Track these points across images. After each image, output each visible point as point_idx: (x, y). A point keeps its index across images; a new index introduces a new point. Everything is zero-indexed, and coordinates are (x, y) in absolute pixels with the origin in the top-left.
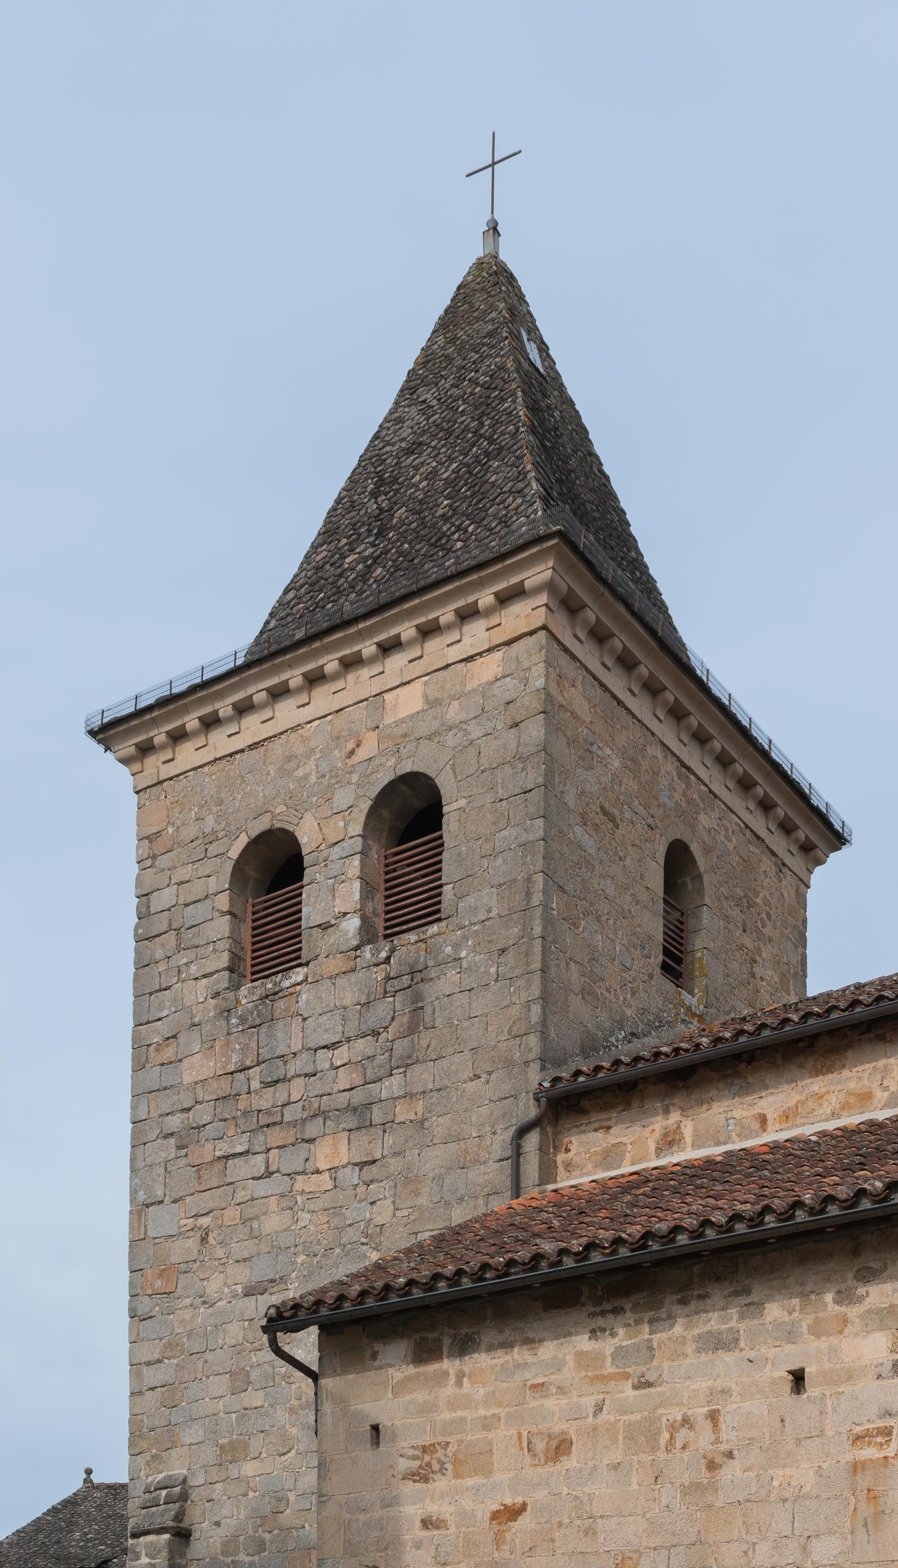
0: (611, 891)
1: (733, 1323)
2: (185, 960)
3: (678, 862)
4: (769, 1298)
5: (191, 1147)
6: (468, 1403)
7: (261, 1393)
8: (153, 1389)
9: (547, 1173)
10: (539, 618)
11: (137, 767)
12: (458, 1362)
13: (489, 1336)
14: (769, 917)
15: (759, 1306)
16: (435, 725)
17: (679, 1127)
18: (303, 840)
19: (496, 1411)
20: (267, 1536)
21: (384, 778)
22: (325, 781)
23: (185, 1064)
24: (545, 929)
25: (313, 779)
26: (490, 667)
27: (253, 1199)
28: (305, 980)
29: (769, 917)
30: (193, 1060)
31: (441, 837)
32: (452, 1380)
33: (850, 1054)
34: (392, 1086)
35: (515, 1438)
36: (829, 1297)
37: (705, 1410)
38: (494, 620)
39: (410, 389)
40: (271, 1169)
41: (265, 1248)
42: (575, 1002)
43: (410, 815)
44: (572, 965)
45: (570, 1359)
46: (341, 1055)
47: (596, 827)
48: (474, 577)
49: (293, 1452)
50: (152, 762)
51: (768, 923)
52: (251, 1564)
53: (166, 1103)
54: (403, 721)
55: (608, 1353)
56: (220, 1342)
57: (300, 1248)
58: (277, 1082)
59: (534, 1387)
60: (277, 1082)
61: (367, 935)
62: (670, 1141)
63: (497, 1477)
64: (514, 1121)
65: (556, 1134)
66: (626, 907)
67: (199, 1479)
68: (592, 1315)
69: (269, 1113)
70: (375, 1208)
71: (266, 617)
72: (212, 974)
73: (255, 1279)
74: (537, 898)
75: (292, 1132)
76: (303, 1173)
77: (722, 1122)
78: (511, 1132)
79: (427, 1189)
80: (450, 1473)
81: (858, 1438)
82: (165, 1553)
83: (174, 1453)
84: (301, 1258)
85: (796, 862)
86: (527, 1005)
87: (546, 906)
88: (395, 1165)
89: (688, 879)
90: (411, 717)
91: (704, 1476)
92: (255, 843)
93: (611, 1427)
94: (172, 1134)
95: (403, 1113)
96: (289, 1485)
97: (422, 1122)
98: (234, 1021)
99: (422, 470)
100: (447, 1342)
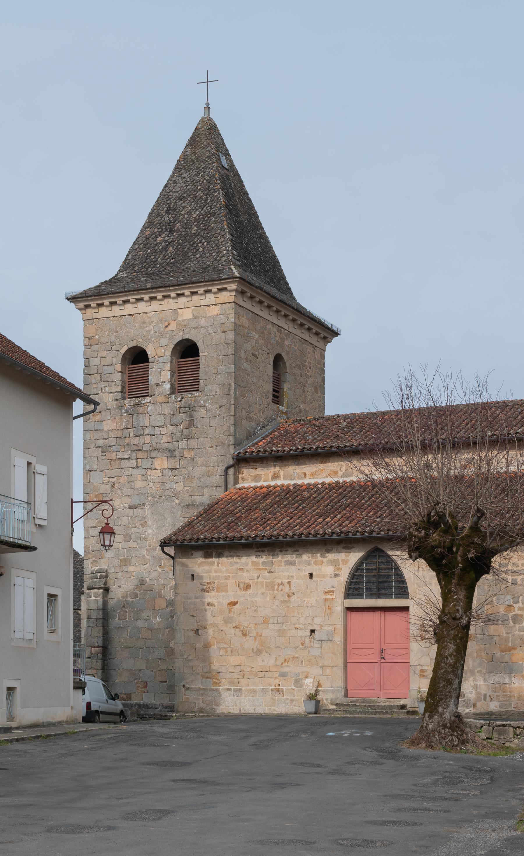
0: (255, 380)
1: (294, 559)
2: (104, 386)
3: (278, 360)
4: (304, 554)
5: (107, 453)
6: (221, 571)
7: (136, 543)
8: (93, 537)
9: (236, 481)
10: (232, 299)
11: (84, 312)
12: (217, 559)
13: (227, 553)
14: (310, 368)
15: (301, 554)
16: (196, 325)
17: (279, 472)
18: (149, 353)
19: (229, 575)
20: (139, 593)
21: (178, 338)
22: (157, 334)
23: (104, 423)
24: (235, 402)
25: (152, 332)
26: (215, 310)
27: (131, 475)
28: (150, 402)
29: (310, 368)
30: (108, 422)
31: (199, 360)
32: (216, 564)
33: (331, 459)
34: (183, 444)
35: (235, 583)
36: (319, 555)
37: (287, 581)
38: (217, 296)
39: (178, 168)
40: (138, 466)
41: (136, 492)
42: (244, 422)
43: (187, 350)
44: (243, 410)
45: (250, 563)
46: (164, 430)
47: (250, 361)
48: (211, 283)
49: (148, 565)
50: (89, 310)
51: (310, 370)
52: (132, 602)
53: (97, 435)
54: (185, 320)
55: (261, 562)
56: (120, 523)
57: (149, 494)
58: (140, 435)
59: (240, 569)
60: (140, 435)
61: (173, 391)
62: (276, 476)
63: (229, 593)
64: (225, 463)
65: (239, 468)
66: (260, 384)
67: (112, 570)
68: (256, 551)
69: (137, 446)
70: (177, 484)
71: (127, 253)
72: (115, 392)
73: (132, 503)
74: (232, 391)
75: (146, 454)
76: (150, 469)
77: (292, 473)
78: (224, 467)
79: (195, 481)
80: (215, 591)
81: (326, 592)
82: (101, 596)
83: (102, 560)
84: (150, 498)
85: (320, 344)
86: (229, 426)
87: (235, 394)
88: (184, 471)
89: (281, 363)
90: (188, 320)
91: (287, 598)
92: (130, 350)
93: (262, 583)
94: (100, 447)
95: (186, 454)
96: (147, 575)
97: (193, 458)
98: (123, 411)
99: (185, 209)
100: (214, 553)
